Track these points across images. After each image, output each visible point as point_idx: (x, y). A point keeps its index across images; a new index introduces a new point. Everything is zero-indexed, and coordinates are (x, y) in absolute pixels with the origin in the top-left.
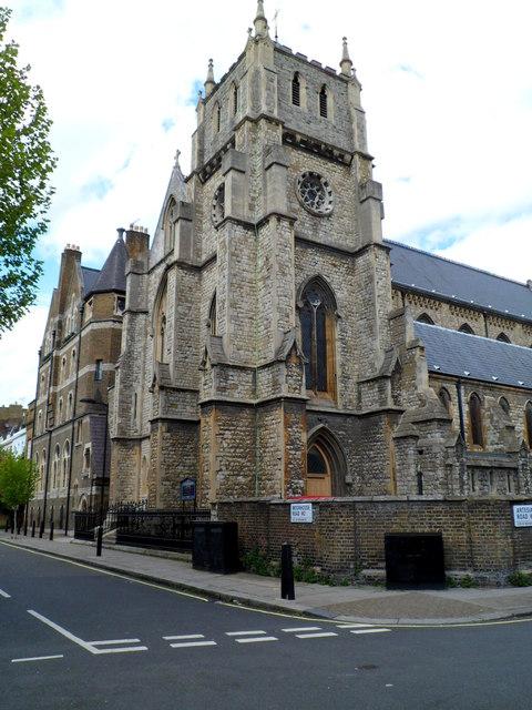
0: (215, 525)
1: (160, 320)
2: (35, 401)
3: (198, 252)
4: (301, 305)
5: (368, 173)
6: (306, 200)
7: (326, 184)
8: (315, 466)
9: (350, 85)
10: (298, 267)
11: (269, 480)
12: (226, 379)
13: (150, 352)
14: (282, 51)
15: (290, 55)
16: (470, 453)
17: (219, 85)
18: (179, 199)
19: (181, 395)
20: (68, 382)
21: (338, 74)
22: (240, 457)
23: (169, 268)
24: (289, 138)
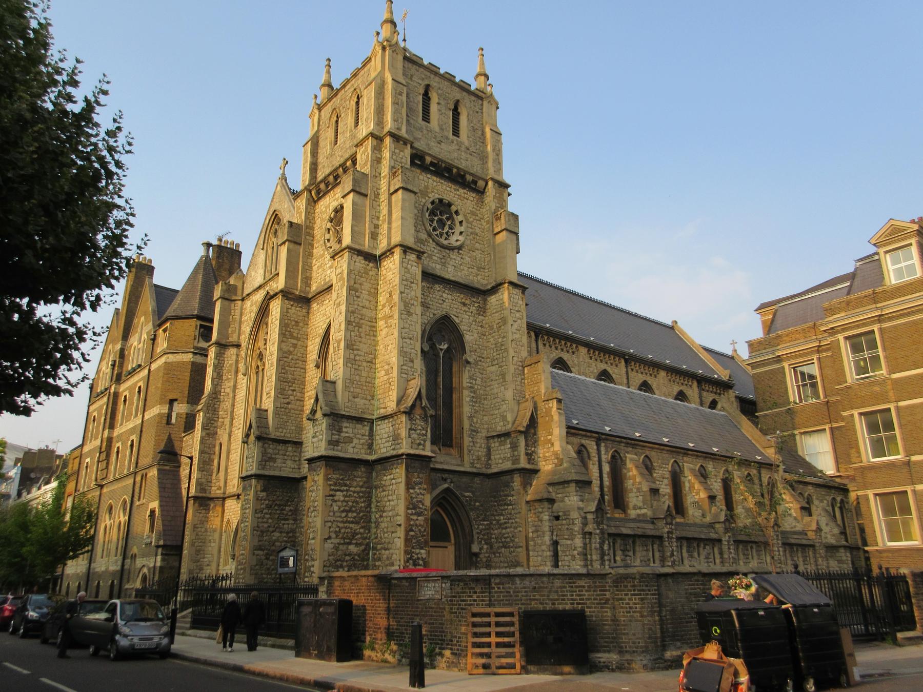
0: (324, 603)
1: (255, 356)
2: (82, 446)
3: (307, 280)
4: (426, 349)
5: (502, 204)
6: (434, 230)
7: (457, 213)
8: (438, 533)
9: (485, 103)
10: (424, 305)
11: (386, 549)
12: (340, 431)
13: (241, 394)
14: (411, 61)
15: (421, 66)
16: (609, 519)
17: (338, 91)
18: (286, 218)
19: (281, 447)
20: (130, 425)
21: (473, 88)
22: (352, 522)
23: (272, 297)
24: (418, 160)
